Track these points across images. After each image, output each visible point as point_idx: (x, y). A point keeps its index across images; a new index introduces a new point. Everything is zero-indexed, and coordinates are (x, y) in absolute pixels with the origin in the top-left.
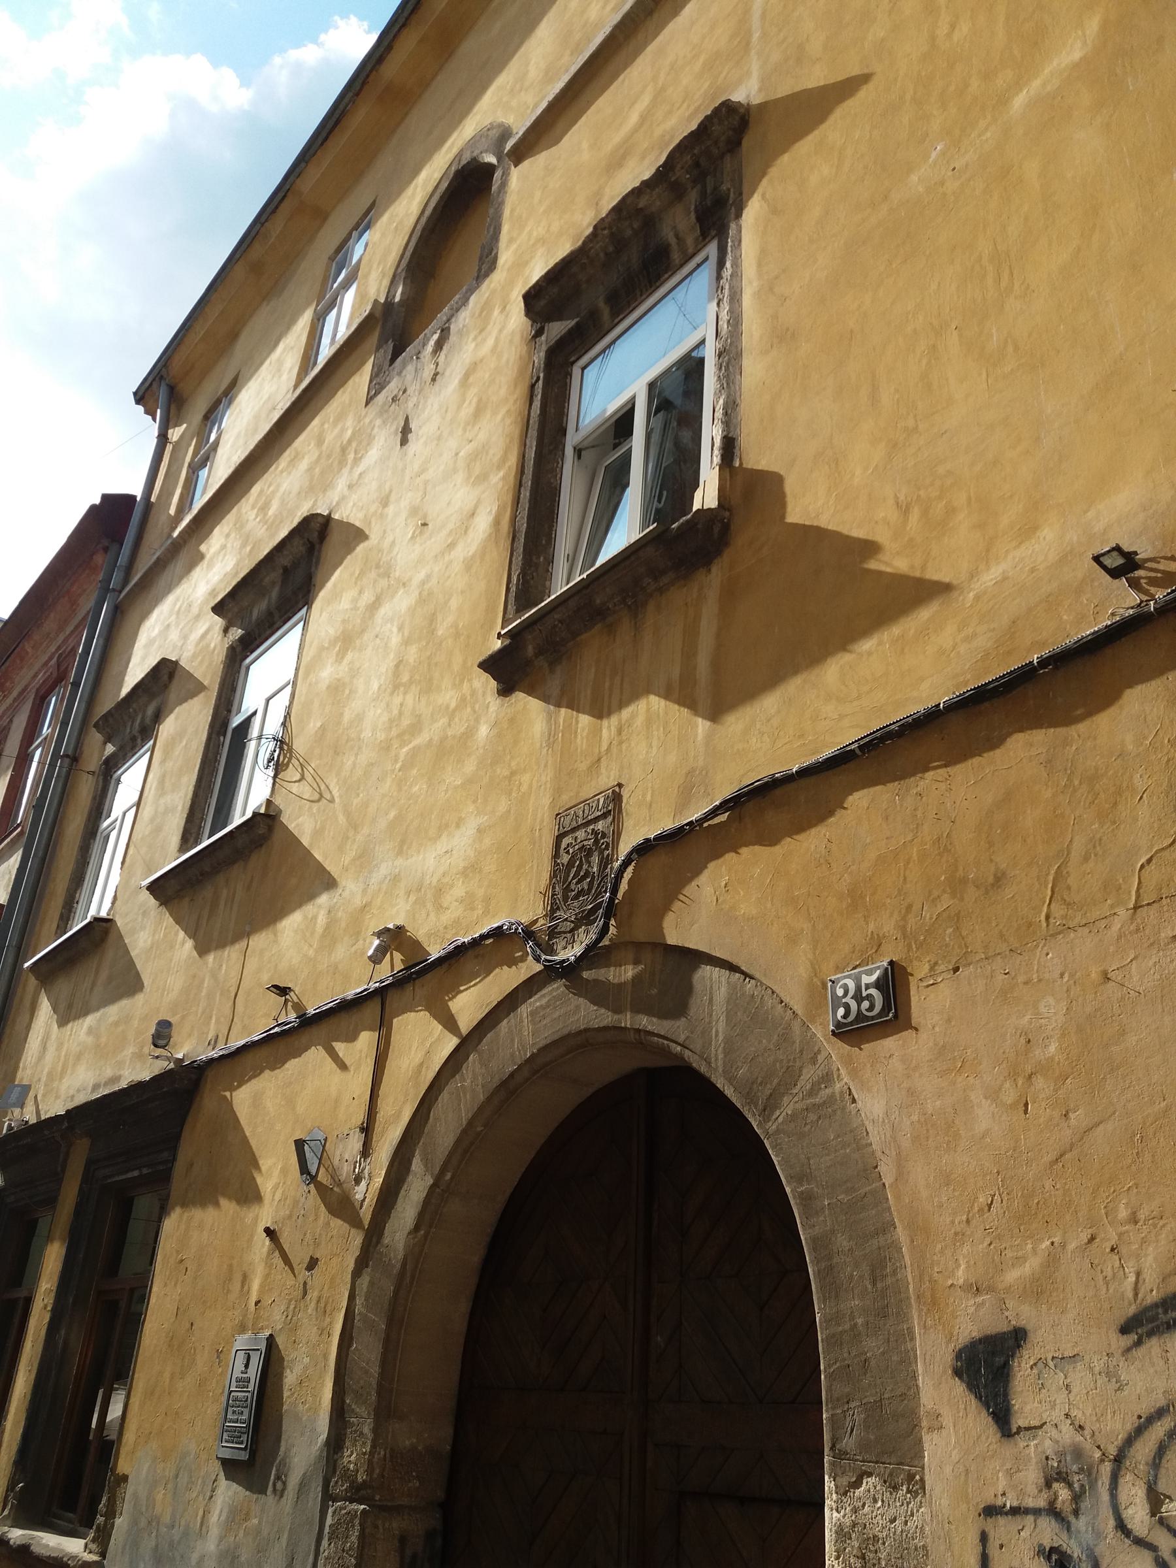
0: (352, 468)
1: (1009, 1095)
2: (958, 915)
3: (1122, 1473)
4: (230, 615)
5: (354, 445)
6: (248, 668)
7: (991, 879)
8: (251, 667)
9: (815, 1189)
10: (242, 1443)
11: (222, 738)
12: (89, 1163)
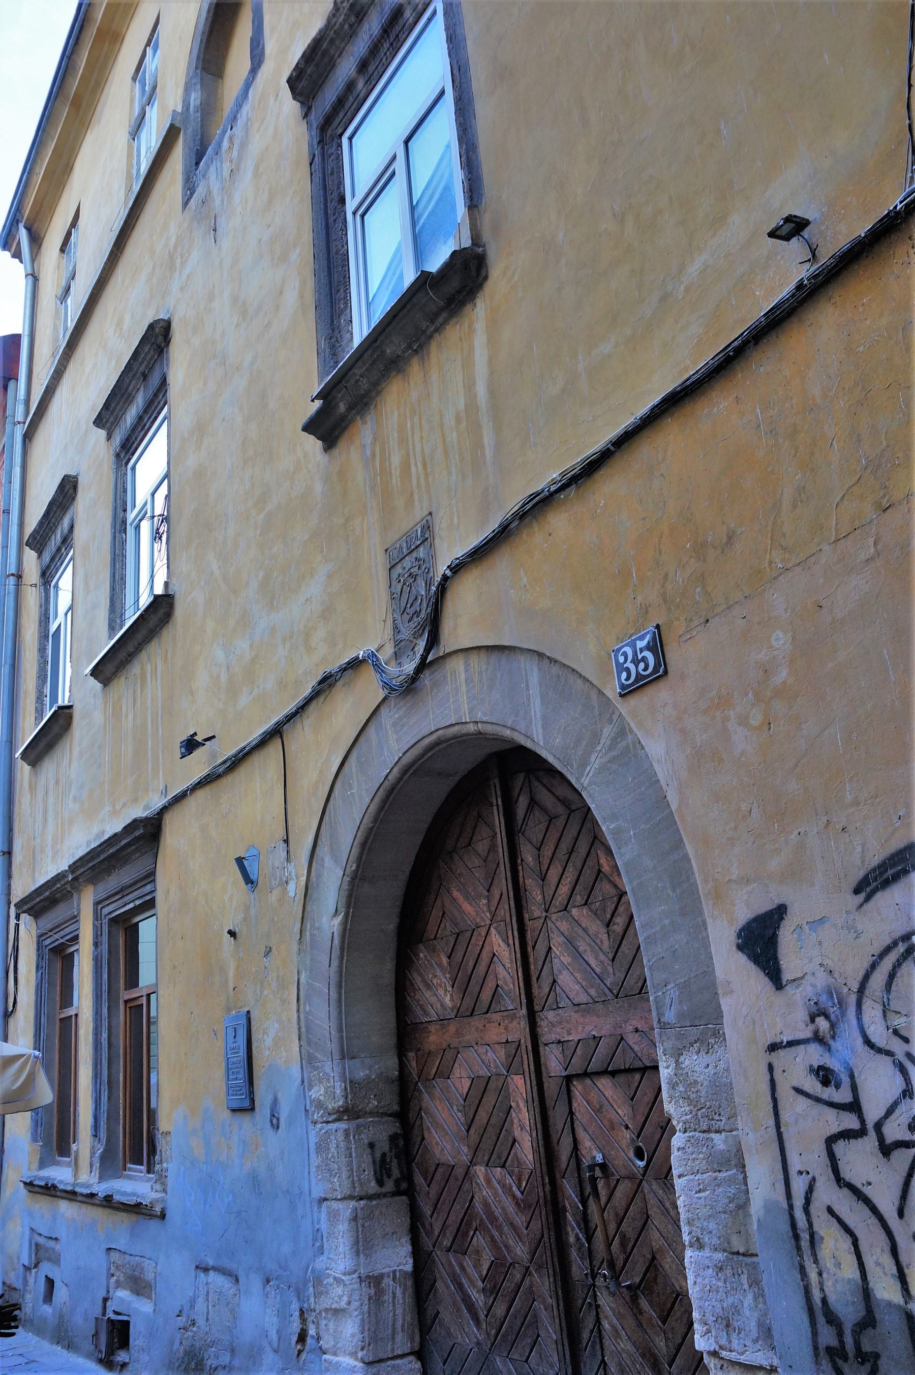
0: (181, 272)
1: (756, 719)
2: (703, 575)
3: (864, 1001)
4: (108, 425)
5: (179, 250)
6: (134, 468)
7: (725, 540)
8: (137, 466)
9: (623, 824)
10: (242, 1094)
11: (124, 535)
12: (97, 903)
